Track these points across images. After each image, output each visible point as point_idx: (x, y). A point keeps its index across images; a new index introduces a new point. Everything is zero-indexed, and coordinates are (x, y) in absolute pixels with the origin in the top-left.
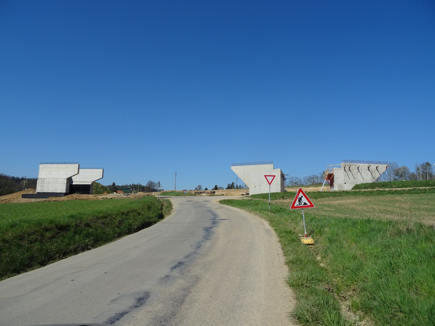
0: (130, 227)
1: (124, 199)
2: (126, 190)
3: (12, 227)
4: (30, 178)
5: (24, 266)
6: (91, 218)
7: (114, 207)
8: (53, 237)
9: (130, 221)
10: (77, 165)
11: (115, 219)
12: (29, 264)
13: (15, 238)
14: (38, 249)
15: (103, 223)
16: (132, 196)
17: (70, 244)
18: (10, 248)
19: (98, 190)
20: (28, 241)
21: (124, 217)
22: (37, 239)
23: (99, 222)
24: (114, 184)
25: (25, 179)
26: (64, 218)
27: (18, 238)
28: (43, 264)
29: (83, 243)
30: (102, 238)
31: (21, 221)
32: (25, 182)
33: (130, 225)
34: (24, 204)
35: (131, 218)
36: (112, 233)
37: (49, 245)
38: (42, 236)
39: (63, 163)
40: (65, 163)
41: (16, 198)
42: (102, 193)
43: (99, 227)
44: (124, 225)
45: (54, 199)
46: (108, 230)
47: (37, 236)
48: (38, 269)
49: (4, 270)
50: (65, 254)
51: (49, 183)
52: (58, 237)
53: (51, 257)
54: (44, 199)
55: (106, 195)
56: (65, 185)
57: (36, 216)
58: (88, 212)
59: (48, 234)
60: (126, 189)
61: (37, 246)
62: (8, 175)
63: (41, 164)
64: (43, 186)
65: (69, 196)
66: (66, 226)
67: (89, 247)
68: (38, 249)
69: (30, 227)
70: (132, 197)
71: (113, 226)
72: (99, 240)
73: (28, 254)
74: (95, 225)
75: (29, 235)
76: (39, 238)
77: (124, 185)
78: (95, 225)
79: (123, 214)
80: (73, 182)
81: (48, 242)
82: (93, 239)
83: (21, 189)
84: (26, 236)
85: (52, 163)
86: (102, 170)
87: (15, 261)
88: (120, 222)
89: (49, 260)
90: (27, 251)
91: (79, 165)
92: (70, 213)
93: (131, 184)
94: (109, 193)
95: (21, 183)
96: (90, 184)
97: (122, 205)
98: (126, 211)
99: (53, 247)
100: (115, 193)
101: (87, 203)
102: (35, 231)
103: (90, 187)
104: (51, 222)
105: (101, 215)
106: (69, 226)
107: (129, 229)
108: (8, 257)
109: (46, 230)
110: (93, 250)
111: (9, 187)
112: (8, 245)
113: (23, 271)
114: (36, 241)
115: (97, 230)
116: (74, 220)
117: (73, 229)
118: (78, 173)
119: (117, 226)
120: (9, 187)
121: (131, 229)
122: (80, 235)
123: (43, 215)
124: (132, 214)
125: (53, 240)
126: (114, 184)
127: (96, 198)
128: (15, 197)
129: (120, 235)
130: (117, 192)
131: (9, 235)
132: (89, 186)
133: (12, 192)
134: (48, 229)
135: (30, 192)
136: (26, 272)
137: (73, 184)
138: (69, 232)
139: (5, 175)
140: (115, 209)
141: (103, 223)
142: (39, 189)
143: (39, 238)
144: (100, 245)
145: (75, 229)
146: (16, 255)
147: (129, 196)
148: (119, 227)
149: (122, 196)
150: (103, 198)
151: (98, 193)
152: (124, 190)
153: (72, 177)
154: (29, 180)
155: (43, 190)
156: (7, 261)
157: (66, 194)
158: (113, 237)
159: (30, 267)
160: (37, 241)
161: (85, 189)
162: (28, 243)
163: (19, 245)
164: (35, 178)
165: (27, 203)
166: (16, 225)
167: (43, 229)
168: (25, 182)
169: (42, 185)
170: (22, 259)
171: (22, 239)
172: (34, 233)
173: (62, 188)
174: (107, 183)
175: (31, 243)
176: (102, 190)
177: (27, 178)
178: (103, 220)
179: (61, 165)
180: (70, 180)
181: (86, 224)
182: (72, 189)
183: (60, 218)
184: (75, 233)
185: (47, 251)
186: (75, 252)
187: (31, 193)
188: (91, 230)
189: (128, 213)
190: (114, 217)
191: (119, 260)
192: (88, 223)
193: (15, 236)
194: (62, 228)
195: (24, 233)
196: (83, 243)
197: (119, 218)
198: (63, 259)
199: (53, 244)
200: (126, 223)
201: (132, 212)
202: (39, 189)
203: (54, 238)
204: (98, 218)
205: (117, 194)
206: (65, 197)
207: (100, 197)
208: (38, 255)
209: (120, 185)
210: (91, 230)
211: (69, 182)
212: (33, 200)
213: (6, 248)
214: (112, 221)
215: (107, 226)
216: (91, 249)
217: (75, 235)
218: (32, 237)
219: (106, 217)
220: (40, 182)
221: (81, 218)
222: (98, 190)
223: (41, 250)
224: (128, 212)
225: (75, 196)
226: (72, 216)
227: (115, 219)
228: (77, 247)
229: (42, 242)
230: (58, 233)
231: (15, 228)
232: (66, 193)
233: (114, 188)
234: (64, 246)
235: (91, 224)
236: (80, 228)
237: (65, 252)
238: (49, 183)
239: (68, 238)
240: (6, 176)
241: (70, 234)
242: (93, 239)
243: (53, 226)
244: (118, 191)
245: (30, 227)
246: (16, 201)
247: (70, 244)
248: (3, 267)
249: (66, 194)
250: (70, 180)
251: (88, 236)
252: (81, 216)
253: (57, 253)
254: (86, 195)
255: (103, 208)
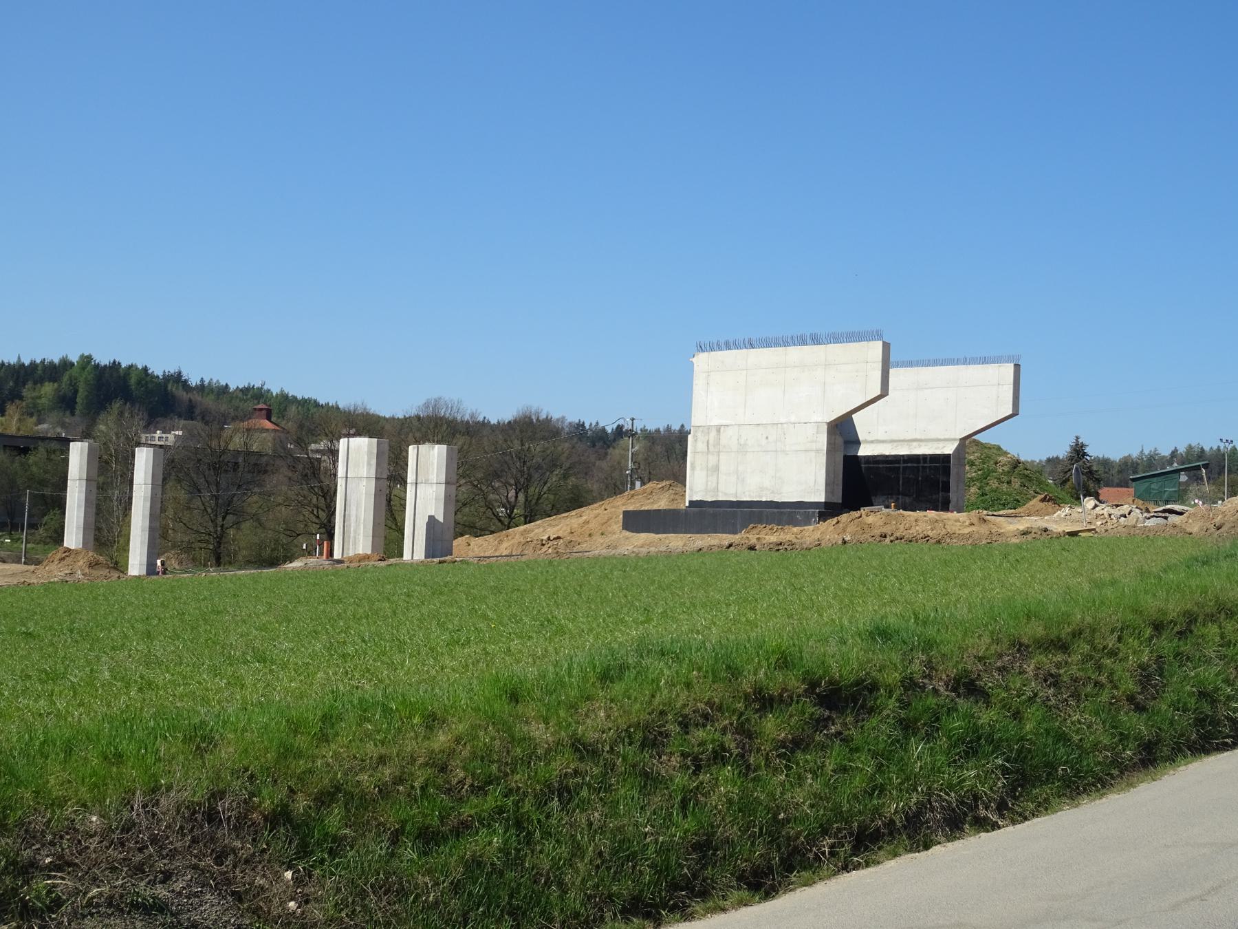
0: (1207, 709)
1: (1149, 537)
2: (1155, 485)
3: (606, 677)
4: (651, 427)
5: (674, 887)
6: (982, 645)
7: (1097, 585)
8: (797, 744)
9: (1210, 674)
10: (878, 346)
11: (1113, 654)
12: (695, 876)
13: (626, 735)
14: (730, 802)
15: (1053, 680)
16: (1196, 515)
17: (882, 789)
18: (608, 789)
19: (994, 484)
20: (683, 755)
21: (1166, 644)
22: (723, 748)
23: (1030, 669)
24: (1078, 451)
25: (631, 434)
26: (843, 642)
27: (639, 736)
28: (761, 884)
29: (951, 787)
30: (1051, 766)
31: (642, 649)
32: (632, 448)
33: (1202, 695)
34: (624, 563)
35: (1210, 652)
36: (1106, 740)
37: (782, 784)
38: (745, 732)
39: (802, 341)
40: (815, 340)
41: (597, 530)
42: (1017, 504)
43: (1032, 700)
44: (1170, 696)
45: (773, 538)
46: (1081, 721)
47: (724, 731)
48: (744, 910)
49: (589, 897)
50: (864, 842)
51: (742, 449)
52: (823, 747)
53: (796, 850)
54: (726, 538)
55: (1038, 513)
56: (823, 459)
57: (705, 626)
58: (962, 612)
59: (772, 727)
60: (1154, 479)
61: (725, 784)
62: (555, 415)
63: (701, 349)
64: (716, 468)
65: (844, 518)
66: (859, 683)
67: (982, 812)
68: (730, 802)
69: (688, 685)
70: (1195, 528)
71: (1104, 698)
72: (1035, 778)
73: (689, 824)
74: (1007, 689)
75: (685, 725)
76: (729, 740)
77: (1135, 454)
78: (1007, 689)
79: (1158, 627)
80: (857, 443)
81: (776, 770)
82: (1005, 771)
83: (615, 488)
84: (673, 728)
85: (751, 345)
86: (1010, 368)
87: (632, 857)
88: (1145, 677)
89: (790, 869)
90: (684, 805)
91: (886, 347)
92: (867, 613)
93: (1182, 449)
94: (1054, 501)
95: (615, 453)
96: (949, 449)
97: (1142, 574)
98: (1174, 608)
99: (800, 795)
100: (1089, 502)
101: (946, 563)
102: (710, 703)
103: (947, 471)
104: (784, 662)
105: (1036, 630)
106: (874, 687)
107: (1200, 722)
108: (602, 829)
109: (764, 701)
110: (1008, 835)
111: (565, 477)
112: (596, 771)
113: (672, 909)
114: (719, 756)
115: (1017, 715)
116: (896, 657)
117: (893, 703)
118: (884, 393)
119: (1131, 699)
120: (565, 477)
121: (1216, 722)
122: (929, 737)
123: (735, 622)
124: (1213, 629)
125: (800, 756)
126: (1078, 451)
127: (984, 530)
128: (593, 525)
129: (1152, 756)
130: (1097, 496)
131: (596, 723)
132: (940, 463)
133: (576, 501)
134: (772, 699)
135: (656, 498)
136: (688, 917)
137: (863, 451)
138: (874, 721)
139: (543, 416)
140: (1109, 592)
141: (1053, 680)
142: (701, 484)
143: (729, 740)
144: (1043, 807)
145: (905, 705)
146: (636, 825)
147: (1173, 519)
148: (1140, 708)
149: (1131, 520)
150: (1025, 533)
151: (995, 502)
152: (1143, 486)
153: (856, 417)
154: (651, 438)
155: (817, 451)
156: (600, 854)
157: (828, 511)
158: (1115, 763)
159: (704, 894)
160: (724, 762)
161: (920, 481)
162: (685, 767)
163: (646, 775)
164: (676, 427)
165: (649, 558)
166: (623, 668)
167: (747, 696)
168: (632, 448)
169: (712, 460)
170: (663, 850)
171: (654, 744)
172: (706, 717)
173: (808, 480)
174: (1037, 444)
175: (698, 769)
176: (1016, 483)
177: (638, 427)
178: (1048, 661)
179: (795, 353)
180: (842, 431)
181: (957, 680)
182: (863, 480)
183: (825, 641)
184: (907, 726)
185: (775, 816)
186: (915, 832)
187: (662, 503)
188: (986, 717)
189: (1188, 625)
190: (1111, 642)
191: (1175, 907)
192: (966, 672)
193: (622, 723)
194: (840, 698)
195: (662, 713)
196: (951, 787)
197: (1138, 654)
198: (857, 867)
199: (800, 779)
200: (1181, 684)
201: (1211, 617)
202: (701, 484)
203: (806, 750)
204: (1020, 648)
205: (1104, 509)
206: (823, 526)
207: (1010, 525)
208: (733, 832)
209: (1116, 455)
210: (986, 717)
211: (839, 440)
212: (676, 541)
213: (589, 786)
214: (1099, 668)
215: (1076, 695)
216: (995, 826)
217: (907, 738)
218: (700, 734)
219: (1063, 647)
220: (701, 446)
221: (928, 645)
222: (994, 484)
223: (745, 807)
224: (1191, 618)
225: (876, 518)
226: (882, 634)
227: (1113, 654)
228: (922, 807)
229: (748, 767)
230: (820, 723)
231: (618, 688)
232: (827, 504)
233: (1081, 476)
234: (855, 797)
235: (987, 682)
236: (932, 701)
237: (863, 828)
238: (742, 449)
239: (875, 755)
240: (548, 421)
241: (879, 728)
242: (1005, 771)
243: (795, 683)
244: (1104, 492)
245: (688, 685)
246: (597, 547)
247: (882, 789)
248: (584, 881)
249: (828, 511)
250: (842, 431)
251: (972, 745)
252: (931, 631)
253: (825, 832)
254: (932, 514)
255: (1052, 591)
